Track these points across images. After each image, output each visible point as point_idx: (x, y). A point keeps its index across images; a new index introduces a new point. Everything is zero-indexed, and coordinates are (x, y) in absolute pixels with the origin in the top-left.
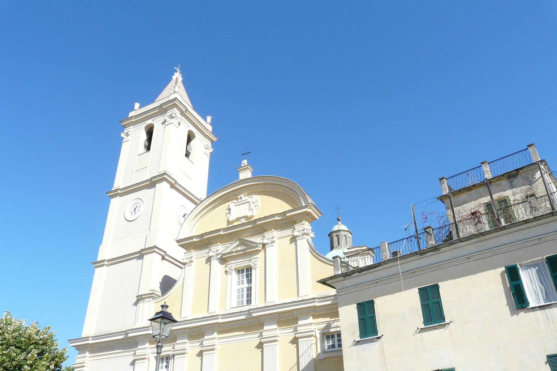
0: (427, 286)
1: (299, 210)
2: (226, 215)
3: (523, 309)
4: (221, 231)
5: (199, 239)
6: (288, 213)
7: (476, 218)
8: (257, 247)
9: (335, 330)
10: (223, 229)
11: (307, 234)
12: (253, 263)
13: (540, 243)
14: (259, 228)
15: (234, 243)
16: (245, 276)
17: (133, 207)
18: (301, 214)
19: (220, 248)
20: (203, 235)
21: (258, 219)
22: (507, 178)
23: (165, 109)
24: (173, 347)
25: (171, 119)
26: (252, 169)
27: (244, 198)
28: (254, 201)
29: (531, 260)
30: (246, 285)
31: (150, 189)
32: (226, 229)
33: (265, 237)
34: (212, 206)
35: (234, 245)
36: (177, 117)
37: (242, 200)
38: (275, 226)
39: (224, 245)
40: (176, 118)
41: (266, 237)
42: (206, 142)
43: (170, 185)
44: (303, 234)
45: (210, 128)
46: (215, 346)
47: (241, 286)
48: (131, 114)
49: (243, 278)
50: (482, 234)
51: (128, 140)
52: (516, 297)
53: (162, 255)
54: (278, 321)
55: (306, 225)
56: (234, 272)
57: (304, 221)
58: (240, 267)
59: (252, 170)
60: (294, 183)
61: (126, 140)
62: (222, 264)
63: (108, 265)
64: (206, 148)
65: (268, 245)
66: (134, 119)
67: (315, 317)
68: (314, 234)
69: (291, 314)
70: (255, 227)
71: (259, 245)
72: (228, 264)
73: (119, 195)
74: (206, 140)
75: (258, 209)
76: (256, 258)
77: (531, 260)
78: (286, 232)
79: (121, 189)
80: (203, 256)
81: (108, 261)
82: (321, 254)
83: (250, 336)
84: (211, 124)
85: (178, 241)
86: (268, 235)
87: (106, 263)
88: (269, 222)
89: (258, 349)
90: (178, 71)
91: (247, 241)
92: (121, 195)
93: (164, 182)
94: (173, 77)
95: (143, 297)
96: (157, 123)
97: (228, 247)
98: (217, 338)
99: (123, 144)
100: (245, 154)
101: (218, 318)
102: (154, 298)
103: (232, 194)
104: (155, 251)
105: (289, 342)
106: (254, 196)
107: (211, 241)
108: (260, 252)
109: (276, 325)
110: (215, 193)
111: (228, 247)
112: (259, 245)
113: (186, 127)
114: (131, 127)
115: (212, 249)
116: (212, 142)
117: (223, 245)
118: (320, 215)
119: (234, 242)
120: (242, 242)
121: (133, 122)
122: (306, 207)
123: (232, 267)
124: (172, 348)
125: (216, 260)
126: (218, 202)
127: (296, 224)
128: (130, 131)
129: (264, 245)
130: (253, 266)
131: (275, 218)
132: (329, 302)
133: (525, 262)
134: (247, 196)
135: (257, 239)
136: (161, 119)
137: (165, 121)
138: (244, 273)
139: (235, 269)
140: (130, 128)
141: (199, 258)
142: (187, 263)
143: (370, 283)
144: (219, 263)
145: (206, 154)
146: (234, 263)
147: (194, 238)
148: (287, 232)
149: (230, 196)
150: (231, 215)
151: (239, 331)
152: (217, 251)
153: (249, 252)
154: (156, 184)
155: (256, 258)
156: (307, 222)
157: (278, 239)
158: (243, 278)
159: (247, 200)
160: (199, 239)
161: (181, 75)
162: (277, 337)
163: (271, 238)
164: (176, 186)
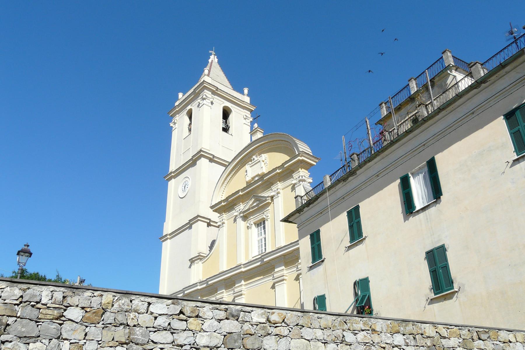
0: (352, 209)
3: (411, 214)
5: (226, 203)
7: (383, 137)
8: (266, 200)
10: (241, 190)
11: (304, 181)
12: (265, 215)
13: (424, 150)
16: (262, 228)
17: (184, 185)
19: (242, 207)
20: (227, 198)
21: (215, 204)
22: (426, 90)
25: (203, 100)
26: (263, 130)
27: (256, 159)
28: (264, 160)
29: (418, 167)
31: (194, 167)
32: (243, 189)
34: (233, 173)
35: (251, 202)
36: (209, 98)
37: (254, 161)
38: (279, 179)
40: (208, 98)
42: (245, 113)
43: (208, 160)
44: (300, 181)
45: (247, 99)
46: (242, 292)
48: (177, 104)
49: (261, 230)
50: (378, 152)
52: (406, 205)
53: (207, 222)
54: (286, 263)
55: (303, 173)
56: (253, 226)
57: (300, 169)
58: (258, 220)
59: (263, 132)
60: (288, 135)
61: (175, 128)
63: (170, 239)
64: (245, 119)
66: (178, 109)
68: (312, 179)
71: (267, 199)
73: (173, 177)
74: (245, 111)
76: (267, 210)
77: (417, 167)
78: (288, 182)
79: (173, 172)
81: (170, 234)
83: (267, 279)
84: (248, 95)
85: (212, 207)
86: (274, 188)
87: (168, 237)
89: (272, 289)
90: (213, 53)
92: (175, 177)
93: (202, 158)
94: (209, 60)
95: (193, 260)
96: (193, 106)
98: (244, 285)
102: (201, 259)
104: (198, 219)
105: (294, 279)
106: (262, 155)
108: (270, 204)
109: (284, 267)
112: (267, 199)
113: (220, 104)
114: (177, 115)
115: (236, 209)
116: (251, 111)
118: (317, 161)
121: (178, 111)
122: (298, 155)
128: (176, 120)
129: (272, 197)
130: (266, 218)
131: (276, 171)
133: (414, 170)
135: (267, 194)
136: (196, 103)
139: (255, 224)
141: (229, 219)
142: (275, 195)
143: (316, 215)
144: (242, 221)
145: (246, 124)
146: (253, 218)
148: (288, 181)
149: (247, 159)
152: (240, 210)
155: (267, 210)
156: (303, 169)
157: (283, 189)
158: (261, 230)
159: (258, 159)
161: (216, 57)
162: (284, 277)
164: (215, 159)
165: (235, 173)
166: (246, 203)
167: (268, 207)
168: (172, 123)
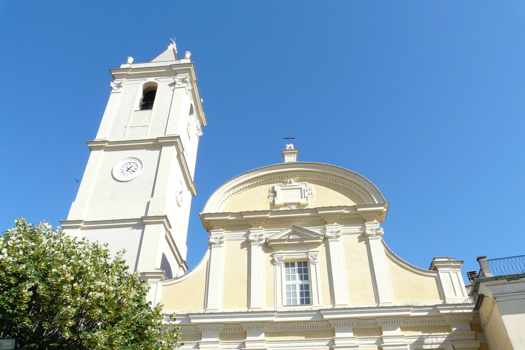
1: (373, 207)
2: (268, 198)
4: (229, 216)
5: (234, 218)
6: (321, 210)
9: (430, 348)
14: (317, 219)
15: (285, 230)
18: (370, 212)
23: (175, 72)
24: (194, 346)
27: (294, 183)
30: (298, 282)
33: (250, 234)
37: (291, 185)
39: (268, 230)
41: (212, 235)
47: (292, 282)
48: (123, 66)
51: (120, 92)
62: (266, 252)
65: (214, 245)
66: (130, 72)
67: (403, 329)
69: (326, 324)
70: (313, 216)
72: (277, 252)
75: (312, 198)
79: (109, 142)
80: (238, 238)
82: (403, 259)
88: (333, 214)
91: (304, 230)
92: (107, 149)
95: (146, 275)
97: (277, 233)
99: (111, 94)
100: (288, 138)
101: (272, 316)
103: (277, 176)
107: (251, 223)
109: (352, 333)
110: (256, 170)
111: (277, 233)
112: (321, 238)
117: (266, 230)
119: (285, 229)
120: (294, 231)
121: (128, 75)
123: (282, 257)
124: (193, 348)
125: (258, 246)
126: (252, 183)
127: (251, 228)
132: (426, 314)
134: (297, 182)
135: (317, 230)
137: (174, 84)
138: (295, 267)
140: (124, 80)
141: (231, 240)
147: (81, 223)
150: (277, 199)
151: (296, 335)
152: (261, 235)
153: (307, 243)
154: (162, 147)
155: (316, 251)
160: (234, 218)
163: (219, 238)
165: (249, 187)
166: (280, 230)
167: (316, 247)
168: (115, 84)
